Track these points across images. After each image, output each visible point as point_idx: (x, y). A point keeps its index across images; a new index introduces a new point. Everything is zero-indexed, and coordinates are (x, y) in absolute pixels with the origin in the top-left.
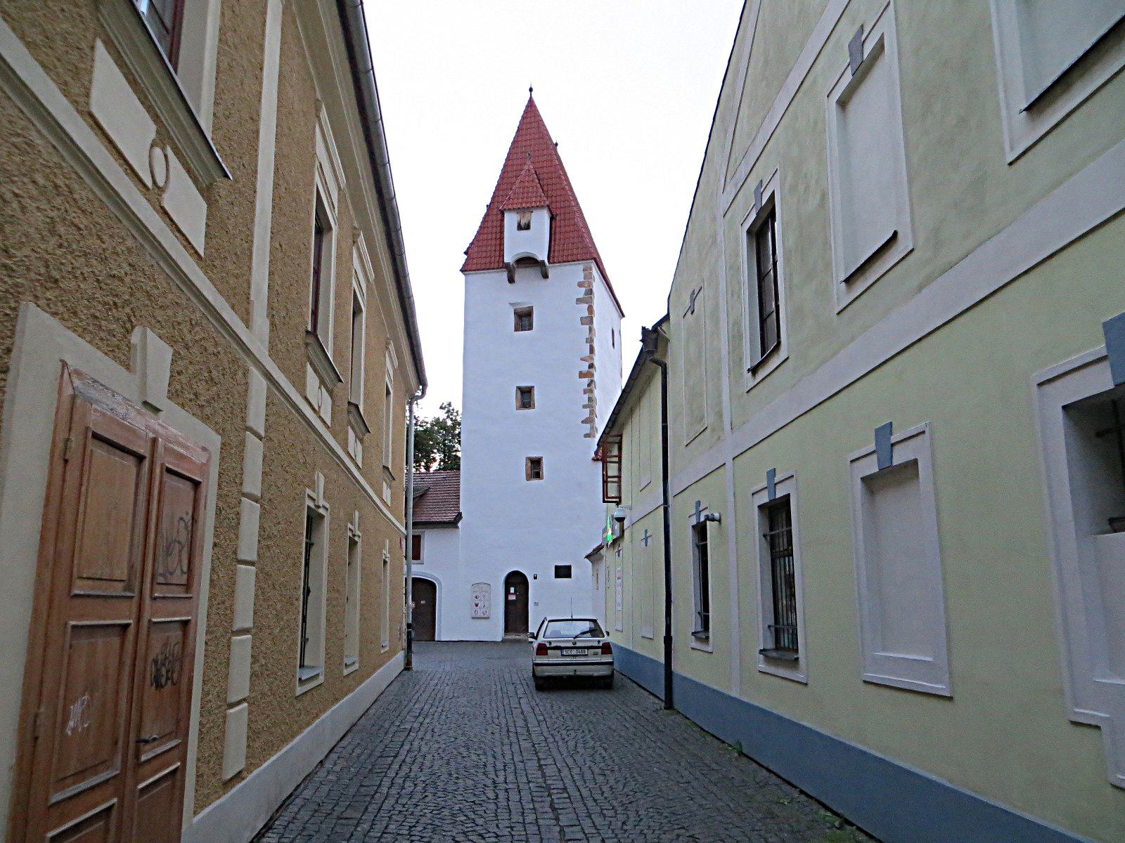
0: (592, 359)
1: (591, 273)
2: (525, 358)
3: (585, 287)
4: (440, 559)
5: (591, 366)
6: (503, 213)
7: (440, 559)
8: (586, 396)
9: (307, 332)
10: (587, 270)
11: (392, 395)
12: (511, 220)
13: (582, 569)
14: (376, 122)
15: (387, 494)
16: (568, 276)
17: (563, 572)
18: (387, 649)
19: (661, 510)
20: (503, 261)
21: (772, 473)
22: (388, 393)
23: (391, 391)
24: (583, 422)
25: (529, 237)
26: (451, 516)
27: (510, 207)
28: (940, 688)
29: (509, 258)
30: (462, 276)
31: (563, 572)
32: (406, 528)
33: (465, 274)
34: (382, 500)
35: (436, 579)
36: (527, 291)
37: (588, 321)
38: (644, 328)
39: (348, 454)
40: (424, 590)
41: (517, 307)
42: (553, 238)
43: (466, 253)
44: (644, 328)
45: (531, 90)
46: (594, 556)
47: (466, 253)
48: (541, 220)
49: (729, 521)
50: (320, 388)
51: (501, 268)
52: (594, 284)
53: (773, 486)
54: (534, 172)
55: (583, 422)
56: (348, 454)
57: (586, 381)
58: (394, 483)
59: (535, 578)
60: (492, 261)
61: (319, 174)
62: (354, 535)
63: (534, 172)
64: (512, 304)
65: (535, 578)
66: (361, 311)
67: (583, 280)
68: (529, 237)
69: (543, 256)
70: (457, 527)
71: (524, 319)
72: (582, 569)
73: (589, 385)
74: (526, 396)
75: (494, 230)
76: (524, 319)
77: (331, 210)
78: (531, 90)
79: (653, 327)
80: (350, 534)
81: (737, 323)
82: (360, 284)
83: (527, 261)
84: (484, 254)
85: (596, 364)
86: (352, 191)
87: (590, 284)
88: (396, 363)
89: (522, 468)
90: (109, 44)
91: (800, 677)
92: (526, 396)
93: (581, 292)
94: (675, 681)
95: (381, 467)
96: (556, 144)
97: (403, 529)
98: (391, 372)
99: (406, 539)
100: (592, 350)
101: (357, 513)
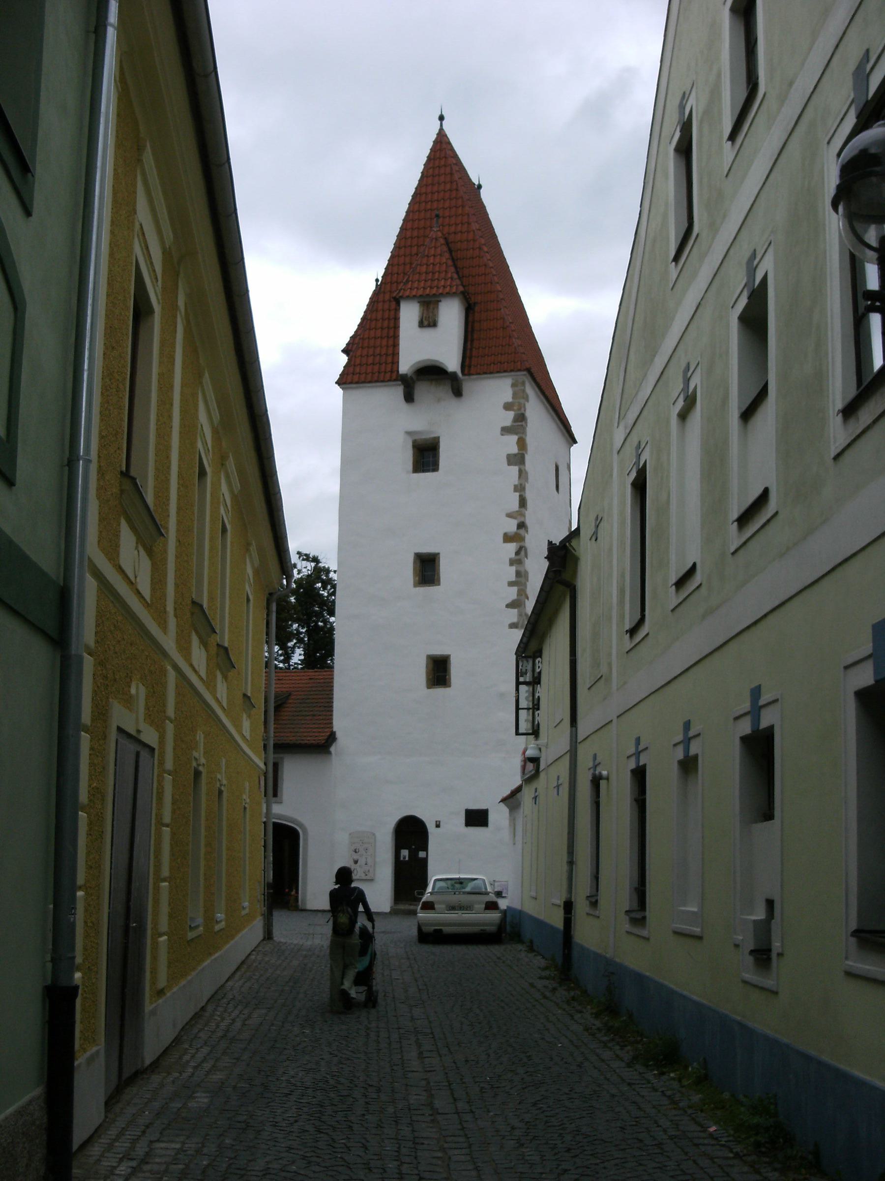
0: (523, 515)
1: (524, 391)
2: (427, 511)
3: (513, 410)
4: (301, 796)
5: (522, 525)
6: (398, 304)
7: (301, 796)
8: (513, 569)
9: (122, 472)
10: (519, 395)
11: (229, 534)
12: (409, 314)
13: (499, 816)
14: (207, 76)
15: (246, 725)
16: (493, 395)
17: (477, 818)
18: (247, 911)
19: (566, 760)
20: (398, 371)
21: (756, 693)
22: (248, 600)
23: (228, 527)
24: (508, 606)
25: (433, 339)
26: (322, 738)
27: (407, 293)
28: (697, 930)
29: (405, 366)
30: (339, 391)
31: (477, 818)
32: (265, 764)
33: (343, 389)
34: (217, 700)
35: (301, 825)
36: (431, 415)
37: (518, 459)
38: (550, 543)
39: (191, 666)
40: (286, 842)
41: (417, 437)
42: (469, 337)
43: (345, 351)
44: (550, 543)
45: (441, 118)
46: (512, 799)
47: (345, 351)
48: (451, 314)
49: (613, 778)
50: (137, 548)
51: (395, 380)
52: (528, 405)
53: (756, 711)
54: (446, 245)
55: (508, 606)
56: (191, 666)
57: (512, 547)
58: (254, 711)
59: (438, 826)
60: (383, 369)
61: (140, 242)
62: (199, 765)
63: (446, 245)
64: (409, 433)
65: (438, 826)
66: (151, 311)
67: (510, 400)
68: (433, 339)
69: (453, 364)
70: (330, 753)
71: (426, 455)
72: (499, 816)
73: (517, 553)
74: (427, 568)
75: (386, 323)
76: (426, 455)
77: (152, 282)
78: (441, 118)
79: (560, 542)
80: (194, 764)
81: (623, 576)
82: (151, 251)
83: (431, 372)
84: (369, 359)
85: (528, 522)
86: (176, 261)
87: (522, 407)
88: (237, 486)
89: (420, 672)
90: (129, 521)
91: (645, 933)
92: (427, 568)
93: (508, 418)
94: (575, 953)
95: (189, 602)
96: (480, 187)
97: (262, 766)
98: (179, 316)
99: (265, 777)
100: (523, 503)
101: (224, 760)
